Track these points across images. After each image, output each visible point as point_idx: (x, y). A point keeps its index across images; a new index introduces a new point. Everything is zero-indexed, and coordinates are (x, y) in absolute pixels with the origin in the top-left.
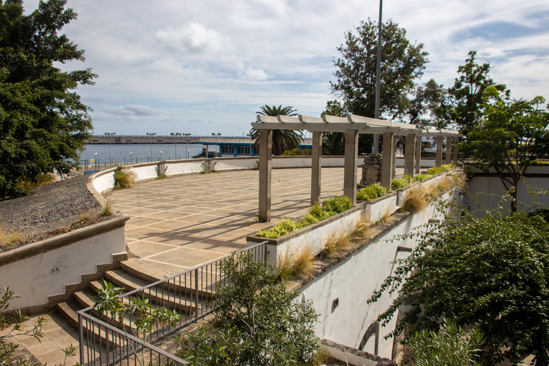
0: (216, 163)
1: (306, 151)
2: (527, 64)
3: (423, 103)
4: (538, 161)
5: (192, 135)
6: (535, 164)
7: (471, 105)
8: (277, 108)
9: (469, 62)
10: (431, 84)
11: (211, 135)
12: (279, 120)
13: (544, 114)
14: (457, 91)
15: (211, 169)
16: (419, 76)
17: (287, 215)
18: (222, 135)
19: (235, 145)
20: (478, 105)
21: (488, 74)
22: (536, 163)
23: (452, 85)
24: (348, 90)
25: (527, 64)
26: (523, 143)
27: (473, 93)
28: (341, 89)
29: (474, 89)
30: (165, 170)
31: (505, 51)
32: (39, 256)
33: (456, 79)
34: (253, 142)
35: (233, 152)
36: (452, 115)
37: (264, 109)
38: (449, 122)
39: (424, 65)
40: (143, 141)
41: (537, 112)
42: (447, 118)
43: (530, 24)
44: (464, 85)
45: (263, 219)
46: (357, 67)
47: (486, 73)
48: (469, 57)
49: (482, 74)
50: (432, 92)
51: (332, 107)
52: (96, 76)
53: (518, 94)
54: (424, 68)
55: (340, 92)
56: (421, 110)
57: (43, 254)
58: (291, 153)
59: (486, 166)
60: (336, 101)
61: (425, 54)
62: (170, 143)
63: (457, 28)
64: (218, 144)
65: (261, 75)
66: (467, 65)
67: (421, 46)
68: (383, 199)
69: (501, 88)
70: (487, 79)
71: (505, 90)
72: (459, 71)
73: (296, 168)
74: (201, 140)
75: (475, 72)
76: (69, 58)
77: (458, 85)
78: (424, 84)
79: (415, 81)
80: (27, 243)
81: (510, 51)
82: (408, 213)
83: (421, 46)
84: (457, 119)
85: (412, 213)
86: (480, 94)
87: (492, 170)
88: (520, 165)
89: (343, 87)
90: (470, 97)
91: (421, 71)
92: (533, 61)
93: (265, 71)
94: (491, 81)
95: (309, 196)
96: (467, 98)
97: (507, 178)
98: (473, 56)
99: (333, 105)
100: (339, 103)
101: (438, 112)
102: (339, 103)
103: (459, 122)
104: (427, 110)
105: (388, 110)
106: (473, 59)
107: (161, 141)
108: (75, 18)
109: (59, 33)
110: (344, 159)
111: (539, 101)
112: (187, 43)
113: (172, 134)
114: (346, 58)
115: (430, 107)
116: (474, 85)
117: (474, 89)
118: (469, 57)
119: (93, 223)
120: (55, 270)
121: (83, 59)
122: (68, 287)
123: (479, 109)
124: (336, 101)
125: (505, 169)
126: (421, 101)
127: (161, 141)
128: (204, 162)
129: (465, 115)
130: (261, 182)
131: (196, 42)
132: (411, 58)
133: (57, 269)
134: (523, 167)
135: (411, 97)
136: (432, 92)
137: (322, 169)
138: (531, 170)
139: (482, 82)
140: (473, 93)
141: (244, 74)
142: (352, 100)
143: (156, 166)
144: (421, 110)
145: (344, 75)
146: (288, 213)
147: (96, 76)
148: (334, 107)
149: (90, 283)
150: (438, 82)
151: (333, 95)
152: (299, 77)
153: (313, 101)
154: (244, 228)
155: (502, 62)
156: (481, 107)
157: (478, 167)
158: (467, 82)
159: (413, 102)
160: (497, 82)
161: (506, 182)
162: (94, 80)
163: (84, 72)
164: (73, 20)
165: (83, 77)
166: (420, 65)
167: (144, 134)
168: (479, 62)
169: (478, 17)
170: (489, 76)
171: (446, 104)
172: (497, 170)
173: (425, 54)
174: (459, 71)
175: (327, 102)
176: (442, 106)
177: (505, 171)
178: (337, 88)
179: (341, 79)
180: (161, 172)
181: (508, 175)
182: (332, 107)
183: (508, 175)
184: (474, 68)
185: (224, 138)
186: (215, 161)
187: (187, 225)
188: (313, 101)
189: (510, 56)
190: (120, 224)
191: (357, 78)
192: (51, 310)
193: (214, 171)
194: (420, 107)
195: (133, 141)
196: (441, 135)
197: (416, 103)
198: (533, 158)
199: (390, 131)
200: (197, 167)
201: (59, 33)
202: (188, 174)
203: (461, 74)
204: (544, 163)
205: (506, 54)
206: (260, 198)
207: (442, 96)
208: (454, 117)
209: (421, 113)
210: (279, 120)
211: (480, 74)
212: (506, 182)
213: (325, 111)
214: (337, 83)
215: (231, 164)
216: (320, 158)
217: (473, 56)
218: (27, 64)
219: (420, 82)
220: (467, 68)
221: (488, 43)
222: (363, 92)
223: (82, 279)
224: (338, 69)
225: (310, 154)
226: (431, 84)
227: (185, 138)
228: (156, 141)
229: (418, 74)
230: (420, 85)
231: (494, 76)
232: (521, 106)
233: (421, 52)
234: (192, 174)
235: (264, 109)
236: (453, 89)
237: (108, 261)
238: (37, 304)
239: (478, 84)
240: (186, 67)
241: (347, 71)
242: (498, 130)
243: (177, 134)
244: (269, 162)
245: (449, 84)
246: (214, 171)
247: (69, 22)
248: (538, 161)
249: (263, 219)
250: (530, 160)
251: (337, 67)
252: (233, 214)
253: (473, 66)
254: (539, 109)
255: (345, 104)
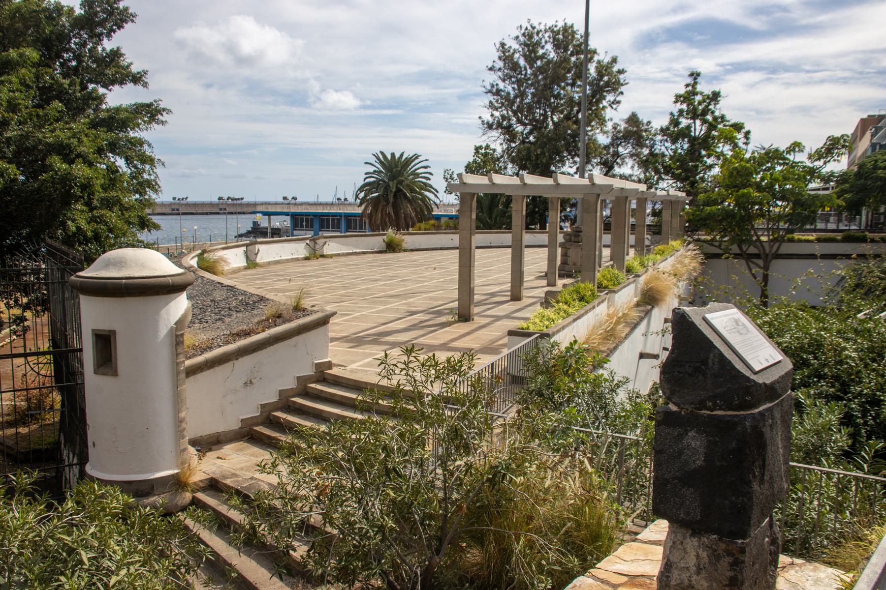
0: (325, 243)
1: (452, 224)
2: (752, 86)
3: (621, 149)
4: (797, 236)
5: (247, 200)
6: (792, 240)
7: (694, 153)
8: (397, 156)
9: (690, 88)
10: (633, 120)
11: (281, 200)
12: (490, 180)
13: (805, 167)
14: (673, 133)
15: (318, 253)
16: (614, 106)
17: (489, 313)
18: (299, 200)
19: (316, 215)
20: (703, 153)
21: (717, 106)
22: (793, 238)
23: (665, 122)
24: (508, 131)
25: (752, 86)
26: (777, 210)
27: (697, 134)
28: (497, 129)
29: (699, 129)
30: (257, 254)
31: (722, 65)
32: (230, 364)
33: (672, 114)
34: (359, 210)
35: (312, 227)
36: (665, 168)
37: (378, 158)
38: (660, 178)
39: (622, 89)
40: (208, 210)
41: (794, 165)
42: (657, 172)
43: (754, 24)
44: (684, 122)
45: (464, 316)
46: (522, 95)
47: (715, 105)
48: (690, 80)
49: (710, 107)
50: (636, 132)
51: (482, 155)
52: (169, 111)
53: (762, 137)
54: (622, 93)
55: (495, 133)
56: (618, 161)
57: (235, 361)
58: (428, 227)
59: (726, 244)
60: (487, 147)
61: (621, 72)
62: (192, 214)
63: (646, 26)
64: (287, 214)
65: (348, 100)
66: (686, 92)
67: (614, 60)
68: (625, 287)
69: (738, 127)
70: (717, 114)
71: (743, 131)
72: (676, 102)
73: (441, 249)
74: (259, 209)
75: (700, 103)
76: (122, 83)
77: (675, 122)
78: (623, 120)
79: (609, 113)
80: (210, 348)
81: (728, 65)
82: (650, 307)
83: (614, 60)
84: (673, 173)
85: (653, 307)
86: (708, 135)
87: (735, 249)
88: (772, 241)
89: (500, 125)
90: (693, 140)
91: (618, 99)
92: (761, 81)
93: (356, 96)
94: (723, 117)
95: (508, 286)
96: (689, 142)
97: (754, 260)
98: (695, 79)
99: (483, 151)
100: (494, 150)
101: (645, 164)
102: (494, 150)
103: (676, 177)
104: (627, 160)
105: (568, 159)
106: (696, 83)
107: (178, 210)
108: (133, 21)
109: (108, 45)
110: (510, 235)
111: (797, 149)
112: (231, 48)
113: (220, 198)
114: (504, 81)
115: (632, 156)
116: (698, 122)
117: (698, 128)
118: (690, 80)
119: (290, 321)
120: (249, 383)
121: (145, 85)
122: (263, 406)
123: (705, 159)
124: (487, 147)
125: (752, 247)
126: (618, 145)
127: (178, 210)
128: (308, 242)
129: (685, 169)
130: (461, 266)
131: (247, 47)
132: (601, 80)
133: (251, 382)
134: (777, 245)
135: (603, 139)
136: (634, 132)
137: (478, 251)
138: (786, 248)
139: (709, 117)
140: (697, 134)
141: (320, 99)
142: (513, 145)
143: (244, 248)
144: (618, 161)
145: (500, 108)
146: (489, 309)
147: (169, 111)
148: (486, 155)
149: (288, 400)
150: (643, 117)
151: (485, 137)
152: (397, 103)
153: (450, 144)
154: (447, 329)
155: (715, 82)
156: (709, 156)
157: (713, 245)
158: (687, 118)
159: (606, 147)
160: (733, 118)
161: (750, 264)
162: (164, 117)
163: (149, 105)
164: (130, 24)
165: (151, 112)
166: (615, 90)
167: (215, 200)
168: (704, 88)
169: (675, 10)
170: (721, 108)
171: (657, 151)
172: (740, 247)
173: (621, 72)
174: (676, 102)
175: (473, 147)
176: (651, 154)
177: (752, 250)
178: (490, 126)
179: (497, 114)
180: (252, 257)
181: (757, 256)
182: (482, 155)
183: (757, 256)
184: (698, 98)
185: (301, 204)
186: (323, 240)
187: (365, 328)
188: (450, 144)
189: (728, 72)
190: (324, 321)
191: (520, 109)
192: (244, 437)
193: (323, 256)
194: (617, 155)
195: (228, 210)
196: (669, 198)
197: (611, 150)
198: (792, 231)
199: (624, 194)
200: (298, 249)
201: (108, 45)
202: (288, 261)
203: (679, 106)
204: (804, 238)
205: (722, 68)
206: (512, 283)
207: (652, 139)
208: (668, 170)
209: (617, 164)
210: (490, 180)
211: (707, 106)
212: (750, 264)
213: (471, 161)
214: (491, 120)
215: (348, 245)
216: (524, 232)
217: (695, 79)
218: (67, 93)
219: (616, 116)
220: (686, 98)
221: (694, 51)
222: (531, 133)
223: (280, 395)
224: (491, 97)
225: (456, 228)
226: (633, 120)
227: (218, 204)
228: (168, 211)
229: (613, 103)
230: (616, 120)
231: (728, 109)
232: (772, 156)
233: (615, 69)
234: (293, 260)
235: (378, 158)
236: (668, 128)
237: (309, 371)
238: (227, 429)
239: (704, 122)
240: (209, 86)
241: (508, 101)
242: (745, 191)
243: (228, 198)
244: (473, 237)
245: (660, 122)
246: (323, 256)
247: (123, 27)
248: (797, 236)
249: (464, 316)
250: (787, 233)
251: (489, 94)
252: (413, 313)
253: (697, 94)
254: (797, 160)
255: (503, 151)
